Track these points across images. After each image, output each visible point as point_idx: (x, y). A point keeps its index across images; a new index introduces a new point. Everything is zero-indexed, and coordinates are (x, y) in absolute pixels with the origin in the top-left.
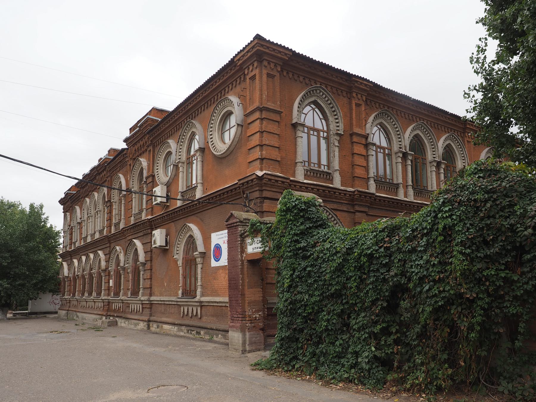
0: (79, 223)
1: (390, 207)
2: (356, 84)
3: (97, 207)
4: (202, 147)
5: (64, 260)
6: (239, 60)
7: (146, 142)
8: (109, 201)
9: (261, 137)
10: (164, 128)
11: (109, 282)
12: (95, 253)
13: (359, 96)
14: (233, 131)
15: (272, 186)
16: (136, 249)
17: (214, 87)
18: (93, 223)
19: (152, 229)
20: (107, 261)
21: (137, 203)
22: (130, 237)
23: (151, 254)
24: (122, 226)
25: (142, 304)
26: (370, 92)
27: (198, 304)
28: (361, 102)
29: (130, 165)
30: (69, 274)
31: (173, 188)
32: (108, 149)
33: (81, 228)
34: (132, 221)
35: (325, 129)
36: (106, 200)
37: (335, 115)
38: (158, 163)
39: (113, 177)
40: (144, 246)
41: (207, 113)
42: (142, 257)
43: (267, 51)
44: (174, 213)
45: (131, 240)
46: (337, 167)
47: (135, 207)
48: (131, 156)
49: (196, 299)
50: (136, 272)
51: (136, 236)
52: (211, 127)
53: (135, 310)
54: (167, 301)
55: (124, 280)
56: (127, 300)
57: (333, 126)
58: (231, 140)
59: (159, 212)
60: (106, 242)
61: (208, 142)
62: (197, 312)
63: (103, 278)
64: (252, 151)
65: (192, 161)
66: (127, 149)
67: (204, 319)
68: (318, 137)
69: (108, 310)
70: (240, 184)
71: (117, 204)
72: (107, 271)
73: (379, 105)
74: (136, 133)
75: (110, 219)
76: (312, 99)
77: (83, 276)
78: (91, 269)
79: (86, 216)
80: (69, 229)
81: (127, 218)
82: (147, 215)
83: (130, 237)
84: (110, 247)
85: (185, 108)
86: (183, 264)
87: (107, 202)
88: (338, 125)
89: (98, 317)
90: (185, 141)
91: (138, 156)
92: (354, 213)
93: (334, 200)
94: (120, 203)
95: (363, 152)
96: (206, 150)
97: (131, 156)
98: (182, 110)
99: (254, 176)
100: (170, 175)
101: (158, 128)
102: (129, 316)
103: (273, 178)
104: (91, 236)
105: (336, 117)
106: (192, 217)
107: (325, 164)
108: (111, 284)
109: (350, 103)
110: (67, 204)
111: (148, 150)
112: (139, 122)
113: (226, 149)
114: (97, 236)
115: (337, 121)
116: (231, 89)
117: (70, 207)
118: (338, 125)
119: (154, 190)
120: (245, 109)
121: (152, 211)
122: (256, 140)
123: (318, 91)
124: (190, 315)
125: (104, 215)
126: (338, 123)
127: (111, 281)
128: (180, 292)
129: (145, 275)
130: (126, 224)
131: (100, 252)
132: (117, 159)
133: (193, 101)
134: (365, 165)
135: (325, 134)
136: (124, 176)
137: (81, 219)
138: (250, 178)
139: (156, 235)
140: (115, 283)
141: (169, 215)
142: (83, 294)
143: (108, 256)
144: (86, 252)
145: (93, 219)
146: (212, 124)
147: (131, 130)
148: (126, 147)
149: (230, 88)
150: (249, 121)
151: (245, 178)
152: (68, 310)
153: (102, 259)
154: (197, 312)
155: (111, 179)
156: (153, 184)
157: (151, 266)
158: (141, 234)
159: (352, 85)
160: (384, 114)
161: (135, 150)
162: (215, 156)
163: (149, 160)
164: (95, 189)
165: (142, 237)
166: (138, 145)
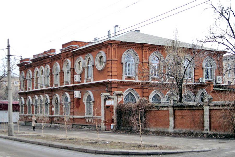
2: (144, 46)
6: (105, 43)
11: (52, 109)
13: (146, 49)
15: (114, 84)
25: (70, 118)
27: (92, 118)
31: (82, 76)
32: (50, 49)
43: (113, 43)
48: (63, 57)
64: (109, 76)
106: (91, 88)
108: (53, 110)
109: (143, 51)
120: (107, 58)
124: (89, 122)
127: (53, 108)
139: (76, 93)
147: (64, 46)
152: (25, 121)
155: (52, 63)
161: (65, 55)
162: (98, 70)
163: (72, 61)
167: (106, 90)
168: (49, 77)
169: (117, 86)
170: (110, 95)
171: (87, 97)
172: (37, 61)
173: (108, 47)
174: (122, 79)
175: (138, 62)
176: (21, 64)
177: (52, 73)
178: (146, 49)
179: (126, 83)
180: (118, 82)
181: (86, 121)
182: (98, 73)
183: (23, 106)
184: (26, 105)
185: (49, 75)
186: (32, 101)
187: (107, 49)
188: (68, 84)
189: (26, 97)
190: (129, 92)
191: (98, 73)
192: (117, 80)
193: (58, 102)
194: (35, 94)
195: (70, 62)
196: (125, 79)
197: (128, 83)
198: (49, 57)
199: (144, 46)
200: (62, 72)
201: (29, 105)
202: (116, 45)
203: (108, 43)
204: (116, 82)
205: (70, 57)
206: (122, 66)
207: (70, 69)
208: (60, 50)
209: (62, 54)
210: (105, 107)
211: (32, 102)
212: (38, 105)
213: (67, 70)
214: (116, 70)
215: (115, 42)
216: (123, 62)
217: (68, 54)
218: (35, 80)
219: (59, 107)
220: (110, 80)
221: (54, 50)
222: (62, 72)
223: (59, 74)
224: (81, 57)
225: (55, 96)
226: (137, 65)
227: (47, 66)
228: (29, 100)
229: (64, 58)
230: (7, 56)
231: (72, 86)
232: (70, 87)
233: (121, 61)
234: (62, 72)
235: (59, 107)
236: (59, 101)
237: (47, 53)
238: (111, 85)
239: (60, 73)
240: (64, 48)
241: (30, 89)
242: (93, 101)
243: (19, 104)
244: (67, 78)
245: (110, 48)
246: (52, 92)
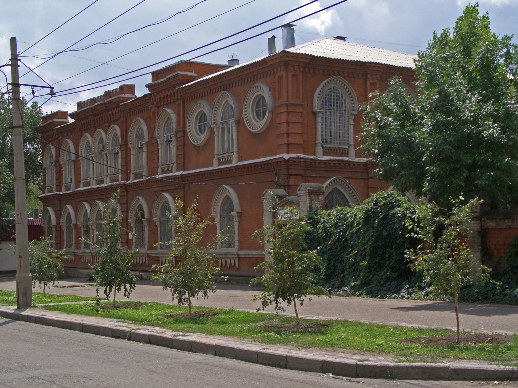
2: (370, 68)
6: (269, 61)
9: (288, 126)
11: (127, 235)
13: (374, 76)
43: (292, 59)
48: (155, 103)
51: (165, 188)
62: (146, 261)
88: (353, 105)
93: (349, 170)
97: (155, 103)
105: (352, 99)
108: (130, 237)
115: (352, 102)
118: (353, 105)
122: (283, 129)
123: (335, 80)
126: (353, 103)
136: (146, 121)
143: (125, 206)
148: (149, 92)
154: (146, 261)
155: (126, 120)
161: (160, 98)
162: (254, 135)
167: (275, 183)
168: (120, 155)
169: (302, 172)
170: (286, 193)
171: (222, 202)
172: (87, 117)
173: (279, 70)
174: (314, 154)
175: (353, 110)
176: (45, 126)
177: (127, 145)
178: (374, 76)
179: (325, 163)
180: (305, 162)
182: (251, 141)
183: (53, 229)
184: (61, 227)
185: (119, 152)
186: (76, 217)
187: (277, 77)
188: (171, 171)
189: (60, 208)
190: (334, 187)
191: (251, 141)
192: (302, 156)
193: (143, 216)
194: (82, 199)
195: (173, 116)
196: (324, 155)
197: (330, 164)
198: (118, 106)
199: (370, 68)
200: (153, 143)
201: (68, 227)
202: (299, 67)
203: (277, 61)
204: (300, 162)
205: (174, 102)
206: (316, 120)
207: (175, 133)
208: (147, 86)
209: (152, 96)
211: (76, 219)
212: (90, 227)
213: (167, 137)
214: (300, 131)
215: (297, 57)
216: (316, 109)
217: (167, 96)
218: (82, 165)
219: (147, 229)
220: (286, 156)
221: (131, 88)
222: (154, 141)
223: (144, 146)
224: (202, 102)
225: (134, 202)
226: (353, 117)
227: (115, 129)
228: (69, 214)
229: (159, 107)
230: (10, 87)
231: (181, 175)
232: (175, 178)
233: (313, 108)
234: (154, 141)
235: (147, 229)
236: (146, 216)
237: (114, 96)
238: (288, 169)
239: (147, 143)
240: (157, 80)
241: (71, 187)
242: (238, 213)
243: (42, 225)
244: (169, 154)
245: (206, 109)
246: (127, 192)
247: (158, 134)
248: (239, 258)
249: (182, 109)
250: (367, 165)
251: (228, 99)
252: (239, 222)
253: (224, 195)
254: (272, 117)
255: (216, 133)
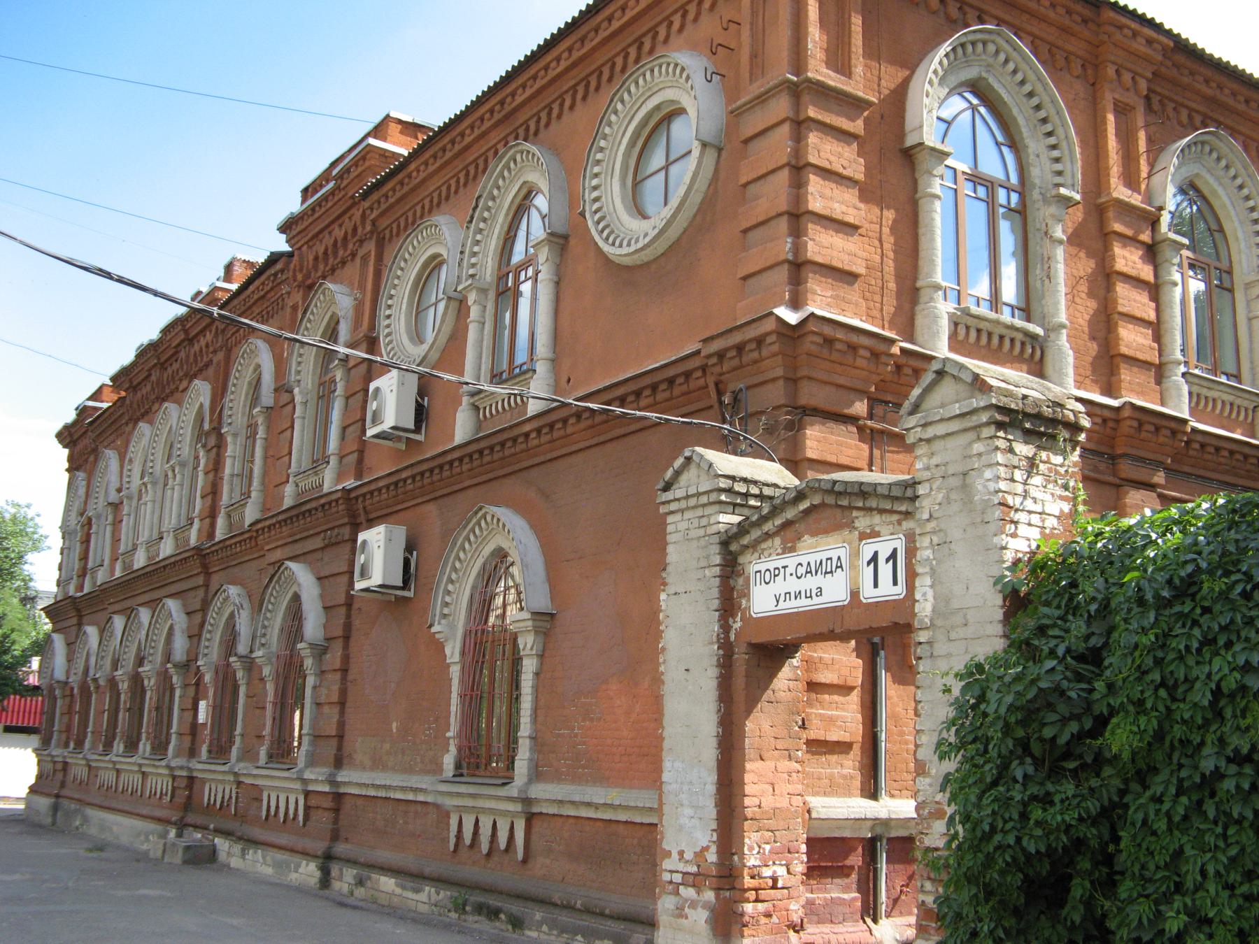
0: (116, 506)
1: (1236, 475)
3: (175, 452)
4: (560, 229)
5: (60, 625)
7: (355, 229)
8: (217, 430)
10: (422, 175)
12: (154, 604)
14: (683, 173)
16: (296, 598)
17: (616, 25)
18: (158, 506)
19: (356, 528)
20: (195, 636)
21: (308, 436)
22: (278, 555)
23: (348, 616)
24: (251, 514)
26: (1163, 70)
28: (1131, 98)
29: (295, 308)
30: (68, 672)
33: (117, 523)
34: (289, 496)
35: (1014, 179)
36: (206, 426)
37: (1050, 134)
38: (391, 297)
39: (235, 350)
40: (322, 587)
41: (577, 119)
42: (313, 626)
44: (441, 467)
45: (280, 563)
46: (1063, 317)
47: (300, 450)
48: (299, 277)
49: (513, 790)
50: (290, 671)
51: (299, 549)
52: (598, 162)
53: (282, 815)
54: (395, 788)
55: (246, 706)
56: (255, 776)
57: (1040, 171)
58: (674, 202)
59: (381, 467)
60: (197, 570)
61: (583, 214)
63: (178, 693)
65: (517, 283)
66: (290, 255)
67: (540, 864)
68: (991, 203)
69: (188, 806)
70: (709, 356)
71: (241, 440)
72: (193, 669)
73: (1190, 117)
74: (325, 198)
75: (213, 492)
76: (971, 73)
77: (113, 683)
78: (140, 661)
79: (136, 482)
80: (80, 531)
81: (272, 487)
82: (340, 477)
83: (278, 555)
84: (206, 585)
85: (502, 103)
86: (463, 653)
87: (208, 434)
88: (1058, 167)
89: (152, 826)
90: (494, 217)
91: (324, 278)
92: (1118, 486)
94: (252, 436)
95: (1147, 273)
96: (572, 242)
97: (299, 277)
98: (492, 111)
99: (769, 325)
100: (430, 336)
101: (400, 176)
102: (258, 833)
103: (840, 335)
104: (148, 550)
105: (1052, 140)
107: (1013, 301)
108: (202, 717)
110: (80, 446)
111: (361, 253)
112: (334, 164)
113: (652, 234)
114: (167, 548)
115: (1055, 153)
116: (681, 29)
117: (90, 454)
118: (1058, 167)
119: (372, 386)
120: (731, 92)
121: (360, 461)
123: (991, 48)
124: (485, 847)
125: (194, 478)
126: (1057, 160)
127: (202, 705)
128: (449, 761)
129: (324, 691)
130: (265, 509)
131: (172, 605)
132: (251, 288)
133: (534, 78)
134: (1152, 316)
135: (1014, 198)
137: (119, 490)
138: (752, 333)
140: (216, 710)
141: (422, 474)
142: (108, 745)
143: (198, 618)
144: (128, 603)
145: (159, 494)
146: (601, 150)
147: (306, 192)
148: (286, 248)
149: (676, 25)
150: (748, 132)
151: (730, 331)
153: (177, 628)
154: (231, 797)
156: (197, 692)
157: (346, 659)
158: (317, 543)
159: (1105, 38)
160: (1207, 149)
161: (316, 258)
163: (362, 287)
164: (172, 393)
165: (318, 555)
166: (328, 240)
181: (264, 813)
199: (1118, 36)
204: (853, 348)
206: (915, 188)
209: (296, 258)
210: (726, 648)
238: (792, 381)
246: (208, 574)
247: (299, 372)
248: (530, 818)
249: (371, 269)
250: (1117, 421)
251: (531, 169)
252: (541, 657)
253: (488, 550)
254: (716, 171)
255: (474, 312)
